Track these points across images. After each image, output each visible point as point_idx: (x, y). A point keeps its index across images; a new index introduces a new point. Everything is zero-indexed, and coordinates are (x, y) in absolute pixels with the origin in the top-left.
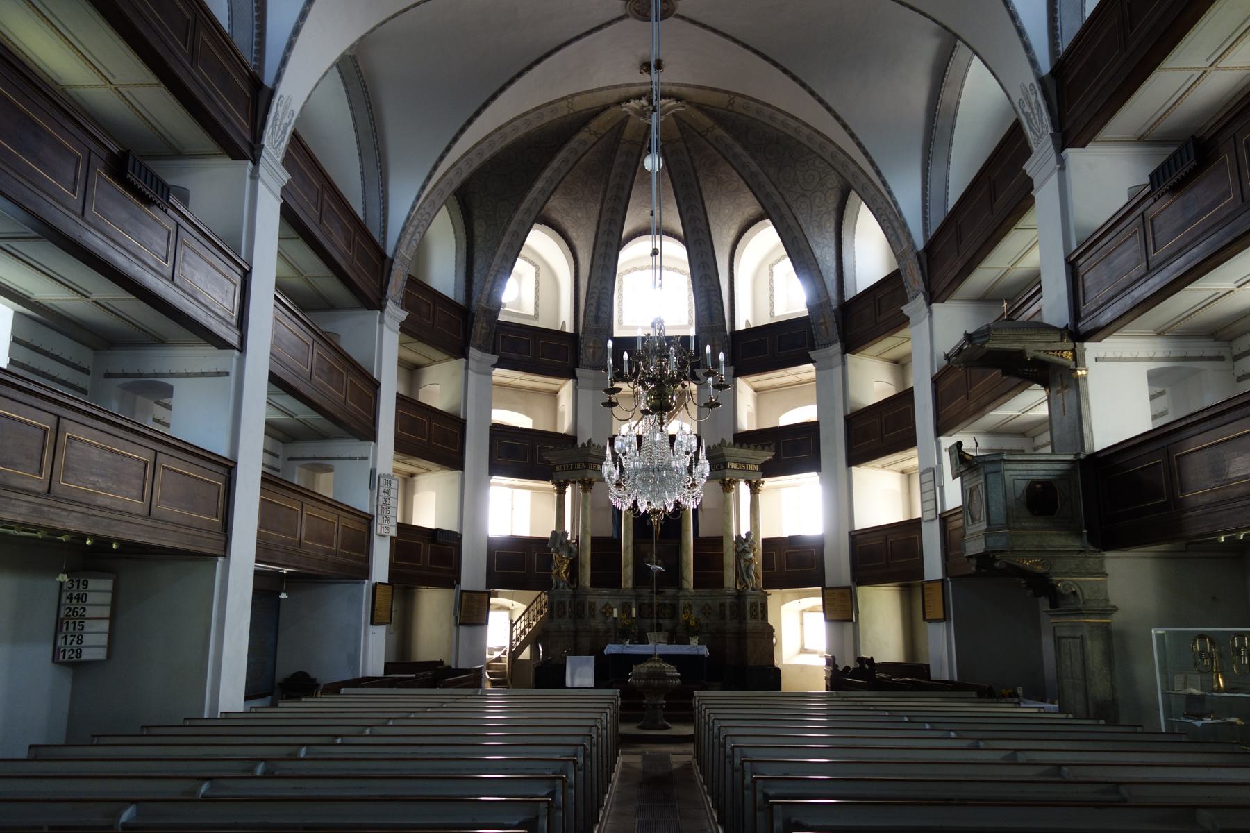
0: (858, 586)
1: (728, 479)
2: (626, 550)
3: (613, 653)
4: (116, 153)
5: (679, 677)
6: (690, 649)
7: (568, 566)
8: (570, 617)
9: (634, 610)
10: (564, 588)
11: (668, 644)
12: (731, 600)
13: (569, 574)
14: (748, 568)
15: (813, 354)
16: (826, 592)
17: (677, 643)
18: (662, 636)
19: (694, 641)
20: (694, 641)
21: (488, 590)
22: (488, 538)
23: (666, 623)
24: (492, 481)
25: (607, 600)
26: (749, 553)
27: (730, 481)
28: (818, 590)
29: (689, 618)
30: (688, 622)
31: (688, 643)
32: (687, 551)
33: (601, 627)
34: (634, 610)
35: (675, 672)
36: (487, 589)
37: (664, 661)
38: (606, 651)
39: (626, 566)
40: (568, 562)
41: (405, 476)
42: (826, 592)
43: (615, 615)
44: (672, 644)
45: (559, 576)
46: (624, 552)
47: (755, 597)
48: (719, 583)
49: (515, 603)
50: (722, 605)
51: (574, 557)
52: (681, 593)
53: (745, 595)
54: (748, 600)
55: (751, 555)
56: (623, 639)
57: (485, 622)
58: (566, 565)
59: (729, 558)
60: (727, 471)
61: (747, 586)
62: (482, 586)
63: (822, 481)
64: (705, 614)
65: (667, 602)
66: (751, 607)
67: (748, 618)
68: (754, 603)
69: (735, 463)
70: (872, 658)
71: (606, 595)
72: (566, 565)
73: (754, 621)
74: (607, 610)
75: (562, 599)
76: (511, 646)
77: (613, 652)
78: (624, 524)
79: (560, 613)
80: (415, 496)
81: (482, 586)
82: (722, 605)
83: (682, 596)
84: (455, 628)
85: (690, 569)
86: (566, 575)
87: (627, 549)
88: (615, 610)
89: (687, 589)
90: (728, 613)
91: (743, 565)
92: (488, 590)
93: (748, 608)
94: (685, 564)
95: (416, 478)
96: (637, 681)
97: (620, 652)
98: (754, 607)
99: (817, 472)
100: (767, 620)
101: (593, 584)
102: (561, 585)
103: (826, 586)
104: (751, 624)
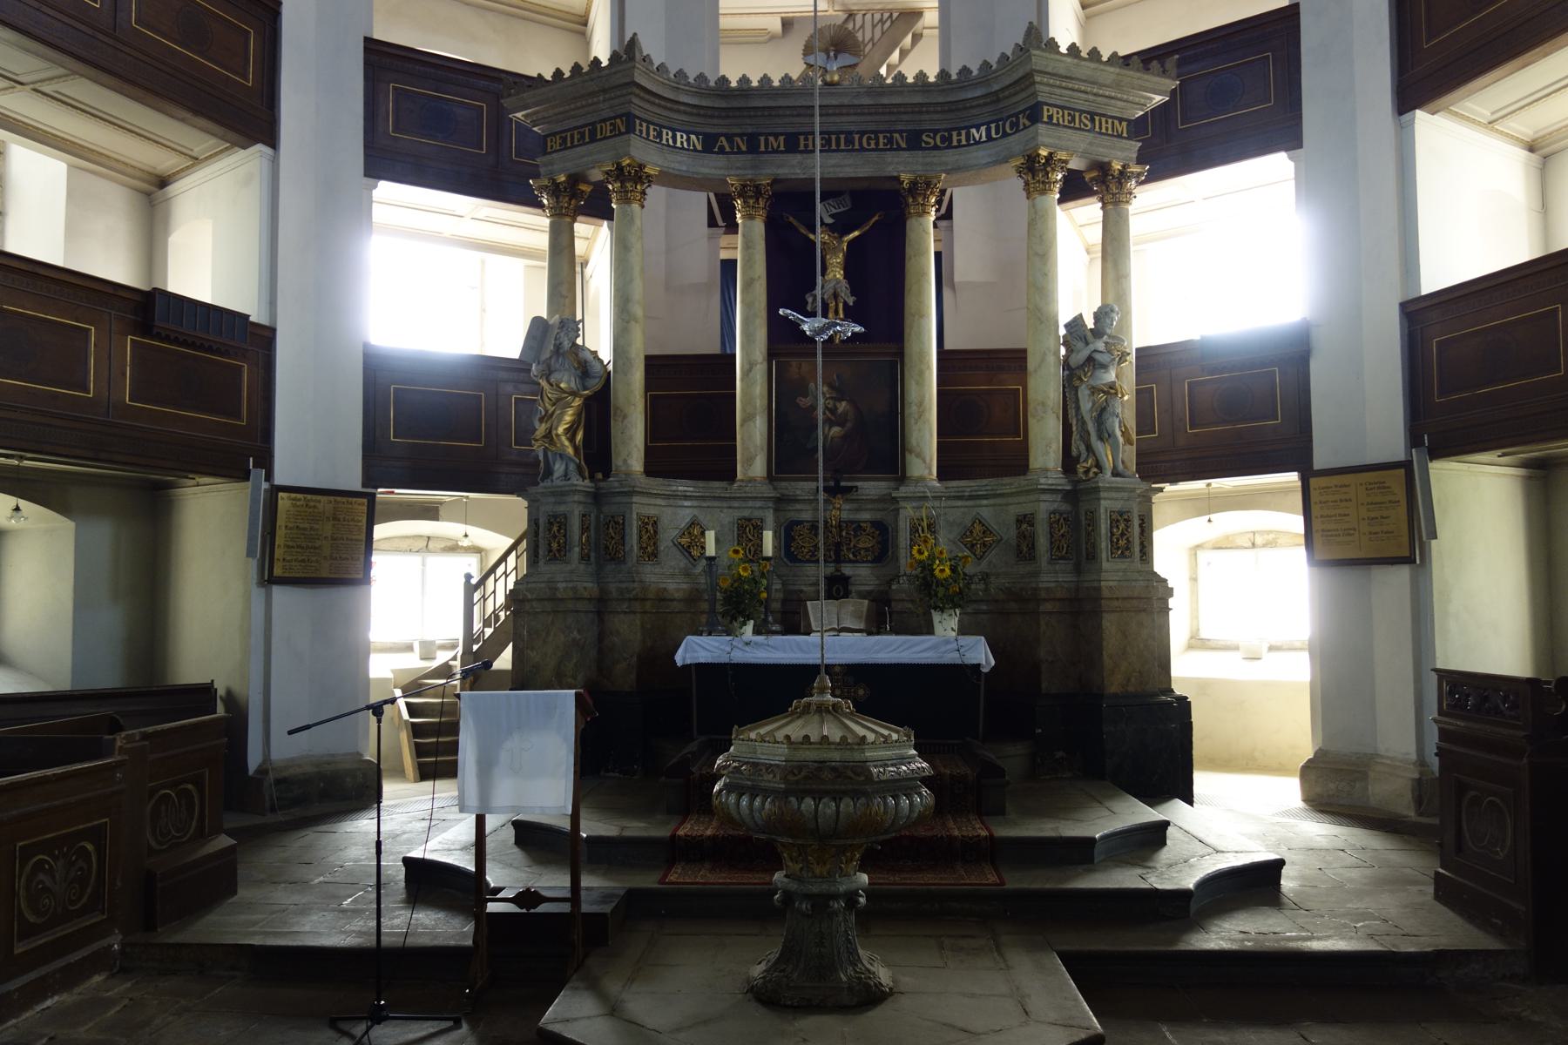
0: (1431, 460)
1: (1044, 153)
2: (746, 374)
3: (702, 660)
5: (926, 781)
6: (934, 647)
7: (578, 415)
8: (584, 558)
9: (768, 537)
10: (566, 476)
11: (870, 633)
12: (1055, 505)
13: (580, 436)
14: (1102, 413)
16: (1314, 482)
17: (896, 631)
18: (852, 610)
19: (946, 625)
20: (946, 625)
22: (366, 346)
23: (862, 574)
24: (375, 193)
25: (696, 512)
26: (1104, 367)
27: (1050, 157)
28: (1284, 490)
29: (932, 557)
30: (927, 567)
31: (930, 631)
32: (921, 373)
33: (676, 586)
34: (768, 537)
35: (904, 760)
36: (364, 485)
37: (866, 709)
38: (680, 658)
39: (749, 418)
40: (577, 402)
41: (145, 186)
42: (1314, 482)
43: (711, 550)
44: (878, 633)
45: (552, 442)
46: (742, 380)
47: (1125, 495)
48: (1017, 462)
49: (471, 530)
50: (1025, 520)
51: (598, 387)
52: (902, 489)
53: (1097, 490)
54: (1102, 502)
55: (1111, 376)
56: (734, 618)
57: (362, 578)
58: (570, 411)
59: (1045, 387)
60: (1041, 128)
61: (1098, 465)
62: (352, 479)
63: (1306, 184)
64: (972, 547)
65: (866, 516)
66: (1114, 523)
67: (1104, 555)
68: (1121, 513)
69: (1063, 108)
71: (686, 498)
72: (570, 411)
73: (1121, 565)
74: (690, 543)
75: (562, 509)
76: (469, 637)
77: (703, 657)
78: (743, 301)
79: (555, 546)
80: (170, 239)
81: (352, 479)
82: (1025, 520)
83: (906, 499)
84: (258, 594)
85: (928, 421)
86: (572, 440)
87: (750, 370)
88: (710, 536)
89: (921, 479)
90: (1042, 542)
91: (1086, 405)
93: (1104, 527)
94: (914, 408)
95: (174, 189)
96: (744, 801)
97: (724, 659)
98: (1122, 526)
99: (1286, 150)
101: (654, 466)
102: (559, 468)
103: (1316, 467)
104: (1111, 572)
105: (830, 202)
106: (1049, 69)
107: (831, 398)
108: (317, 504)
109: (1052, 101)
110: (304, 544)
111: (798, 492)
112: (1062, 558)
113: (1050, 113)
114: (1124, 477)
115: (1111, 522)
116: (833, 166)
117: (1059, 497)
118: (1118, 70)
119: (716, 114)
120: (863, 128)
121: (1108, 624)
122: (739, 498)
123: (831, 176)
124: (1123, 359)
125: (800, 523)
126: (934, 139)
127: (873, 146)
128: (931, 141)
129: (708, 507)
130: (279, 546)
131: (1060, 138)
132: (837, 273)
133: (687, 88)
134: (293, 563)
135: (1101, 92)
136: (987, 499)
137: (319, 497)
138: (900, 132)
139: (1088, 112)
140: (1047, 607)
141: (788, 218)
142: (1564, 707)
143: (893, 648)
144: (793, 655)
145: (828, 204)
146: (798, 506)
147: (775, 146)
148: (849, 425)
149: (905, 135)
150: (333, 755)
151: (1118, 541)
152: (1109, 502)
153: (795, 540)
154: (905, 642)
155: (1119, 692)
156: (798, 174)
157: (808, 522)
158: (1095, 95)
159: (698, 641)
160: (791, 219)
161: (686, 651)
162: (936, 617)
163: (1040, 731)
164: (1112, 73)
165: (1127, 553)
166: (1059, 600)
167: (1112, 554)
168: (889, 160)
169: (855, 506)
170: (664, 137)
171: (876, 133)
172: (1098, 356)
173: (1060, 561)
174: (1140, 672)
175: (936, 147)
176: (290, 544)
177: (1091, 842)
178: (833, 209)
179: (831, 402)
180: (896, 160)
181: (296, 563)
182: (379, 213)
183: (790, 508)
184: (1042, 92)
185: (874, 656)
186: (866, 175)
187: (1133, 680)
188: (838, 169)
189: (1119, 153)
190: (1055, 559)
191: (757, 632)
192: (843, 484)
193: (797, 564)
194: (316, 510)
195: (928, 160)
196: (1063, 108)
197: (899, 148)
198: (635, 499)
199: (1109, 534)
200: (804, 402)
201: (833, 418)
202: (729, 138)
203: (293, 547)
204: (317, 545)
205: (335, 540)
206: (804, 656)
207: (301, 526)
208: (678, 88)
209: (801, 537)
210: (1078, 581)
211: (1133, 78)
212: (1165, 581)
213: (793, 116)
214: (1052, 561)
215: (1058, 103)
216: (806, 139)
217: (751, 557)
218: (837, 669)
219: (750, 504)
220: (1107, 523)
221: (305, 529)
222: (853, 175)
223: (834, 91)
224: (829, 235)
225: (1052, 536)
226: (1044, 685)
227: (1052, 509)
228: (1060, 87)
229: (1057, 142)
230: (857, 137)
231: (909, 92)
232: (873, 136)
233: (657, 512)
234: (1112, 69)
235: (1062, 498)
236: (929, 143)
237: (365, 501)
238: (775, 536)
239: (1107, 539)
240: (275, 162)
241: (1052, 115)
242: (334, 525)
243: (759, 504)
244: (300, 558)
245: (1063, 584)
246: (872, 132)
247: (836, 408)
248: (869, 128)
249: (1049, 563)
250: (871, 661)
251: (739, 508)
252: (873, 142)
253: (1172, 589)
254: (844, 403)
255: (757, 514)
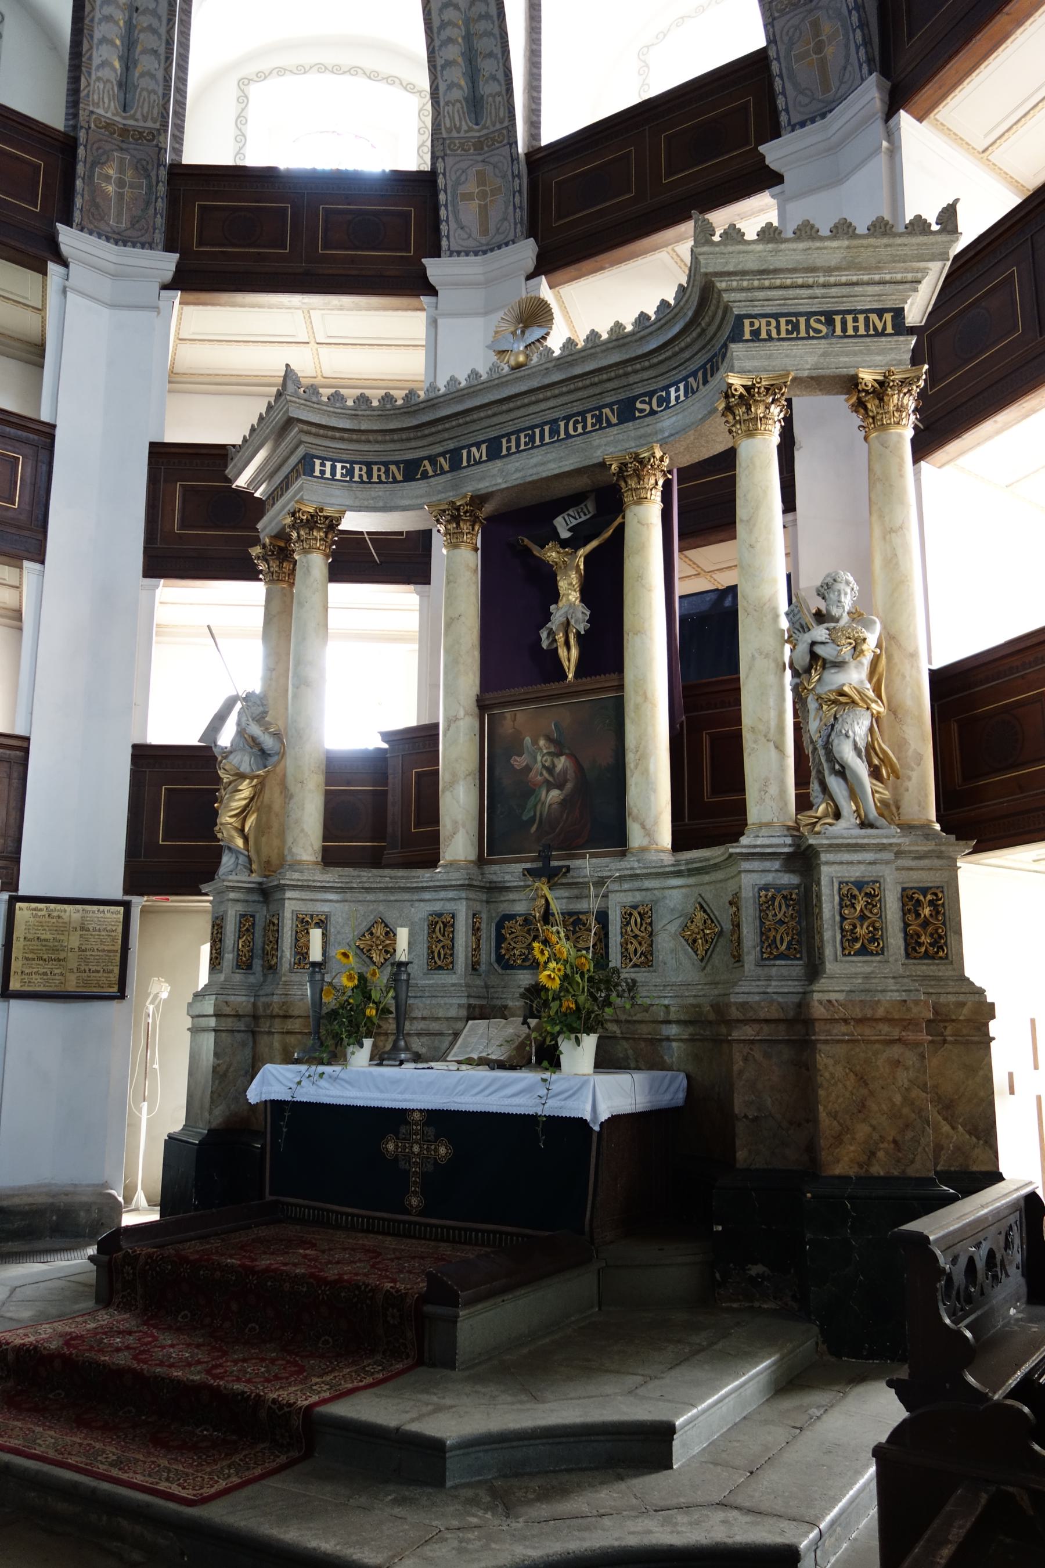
4: (521, 148)
15: (773, 153)
21: (127, 898)
54: (825, 869)
66: (847, 899)
67: (828, 952)
68: (859, 885)
70: (994, 1039)
73: (860, 966)
87: (449, 726)
92: (127, 898)
100: (956, 961)
105: (571, 512)
106: (730, 268)
107: (549, 753)
108: (62, 914)
109: (757, 311)
110: (45, 956)
111: (508, 877)
112: (781, 956)
113: (757, 326)
114: (877, 828)
115: (841, 900)
116: (536, 466)
117: (777, 865)
118: (846, 243)
119: (412, 435)
120: (569, 412)
121: (830, 1062)
122: (427, 887)
123: (535, 477)
124: (858, 649)
125: (511, 917)
126: (650, 404)
127: (580, 430)
128: (647, 407)
129: (396, 901)
130: (17, 958)
131: (770, 357)
132: (574, 596)
133: (368, 413)
134: (34, 976)
135: (832, 280)
136: (707, 873)
137: (65, 906)
138: (610, 405)
139: (821, 313)
140: (748, 1032)
141: (523, 541)
142: (947, 1321)
143: (481, 1087)
144: (368, 1094)
145: (569, 515)
146: (512, 896)
147: (477, 456)
148: (569, 786)
149: (615, 407)
150: (76, 1185)
151: (855, 927)
152: (837, 867)
153: (506, 939)
154: (494, 1080)
155: (851, 1174)
156: (500, 484)
157: (520, 915)
158: (824, 286)
159: (275, 1072)
160: (526, 541)
161: (263, 1082)
162: (565, 1046)
163: (720, 1228)
164: (838, 248)
165: (873, 947)
166: (767, 1021)
167: (843, 949)
168: (596, 443)
169: (576, 892)
170: (357, 472)
171: (583, 414)
172: (819, 650)
173: (778, 962)
174: (895, 1142)
175: (653, 413)
176: (30, 956)
177: (434, 1448)
178: (572, 520)
179: (549, 758)
180: (604, 441)
181: (38, 977)
182: (335, 619)
183: (503, 899)
184: (735, 302)
185: (458, 1099)
186: (572, 468)
187: (881, 1154)
188: (540, 469)
189: (879, 358)
190: (768, 959)
191: (379, 1058)
192: (554, 863)
193: (508, 972)
194: (60, 920)
195: (642, 431)
196: (776, 316)
197: (610, 425)
198: (289, 894)
199: (838, 918)
200: (519, 762)
201: (551, 779)
202: (432, 460)
203: (33, 959)
204: (62, 957)
205: (83, 951)
206: (376, 1095)
207: (43, 937)
208: (357, 415)
209: (513, 936)
210: (804, 993)
211: (877, 247)
212: (981, 992)
213: (489, 417)
214: (762, 962)
215: (768, 310)
216: (509, 441)
217: (439, 963)
218: (417, 1116)
219: (442, 894)
220: (833, 902)
221: (46, 940)
222: (556, 472)
223: (522, 373)
224: (558, 552)
225: (762, 923)
226: (741, 1155)
227: (763, 882)
228: (762, 288)
229: (766, 363)
230: (562, 424)
231: (603, 351)
232: (580, 419)
233: (326, 910)
234: (835, 244)
235: (781, 866)
236: (644, 410)
237: (121, 909)
238: (411, 935)
239: (833, 926)
240: (42, 574)
241: (759, 328)
242: (81, 936)
243: (451, 894)
244: (42, 971)
245: (775, 996)
246: (578, 414)
247: (554, 766)
248: (575, 410)
249: (757, 965)
250: (453, 1107)
251: (429, 900)
252: (580, 426)
253: (992, 1005)
254: (563, 759)
255: (450, 907)
